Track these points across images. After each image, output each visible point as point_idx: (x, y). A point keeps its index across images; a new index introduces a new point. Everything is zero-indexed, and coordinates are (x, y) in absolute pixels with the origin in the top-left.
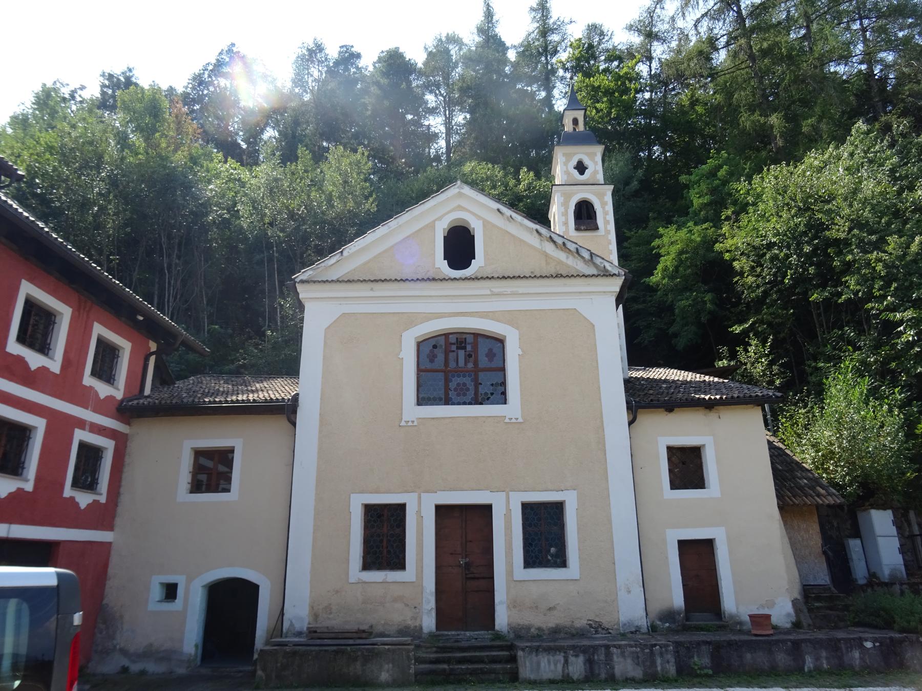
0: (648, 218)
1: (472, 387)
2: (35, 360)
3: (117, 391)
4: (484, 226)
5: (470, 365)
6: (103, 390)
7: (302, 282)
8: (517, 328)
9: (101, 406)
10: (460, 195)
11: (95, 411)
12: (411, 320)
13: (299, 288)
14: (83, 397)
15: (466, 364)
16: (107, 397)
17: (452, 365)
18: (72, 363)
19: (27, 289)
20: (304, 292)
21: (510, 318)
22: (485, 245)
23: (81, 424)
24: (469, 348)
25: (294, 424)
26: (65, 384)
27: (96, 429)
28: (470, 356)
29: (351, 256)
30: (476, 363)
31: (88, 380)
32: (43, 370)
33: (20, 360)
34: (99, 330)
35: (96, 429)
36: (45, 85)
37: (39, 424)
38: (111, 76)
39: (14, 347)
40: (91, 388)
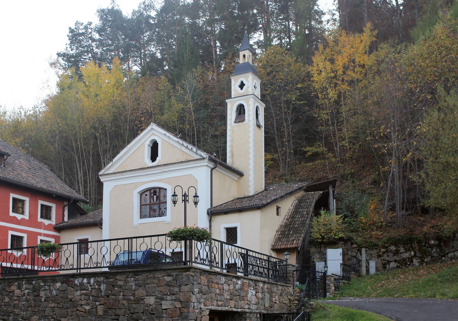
0: (455, 19)
1: (158, 210)
2: (19, 217)
3: (53, 222)
4: (162, 141)
5: (158, 201)
6: (46, 222)
7: (101, 175)
8: (171, 185)
9: (47, 228)
10: (152, 129)
11: (44, 229)
12: (136, 185)
13: (100, 178)
14: (40, 226)
15: (157, 201)
16: (48, 225)
17: (152, 202)
18: (33, 215)
19: (12, 195)
20: (102, 179)
21: (167, 181)
22: (162, 150)
23: (40, 234)
24: (157, 194)
25: (102, 229)
26: (32, 222)
27: (45, 235)
28: (158, 197)
29: (116, 162)
30: (160, 201)
31: (40, 220)
32: (23, 219)
33: (15, 217)
34: (40, 202)
35: (45, 235)
36: (70, 28)
37: (25, 236)
38: (103, 11)
39: (12, 214)
40: (41, 222)
